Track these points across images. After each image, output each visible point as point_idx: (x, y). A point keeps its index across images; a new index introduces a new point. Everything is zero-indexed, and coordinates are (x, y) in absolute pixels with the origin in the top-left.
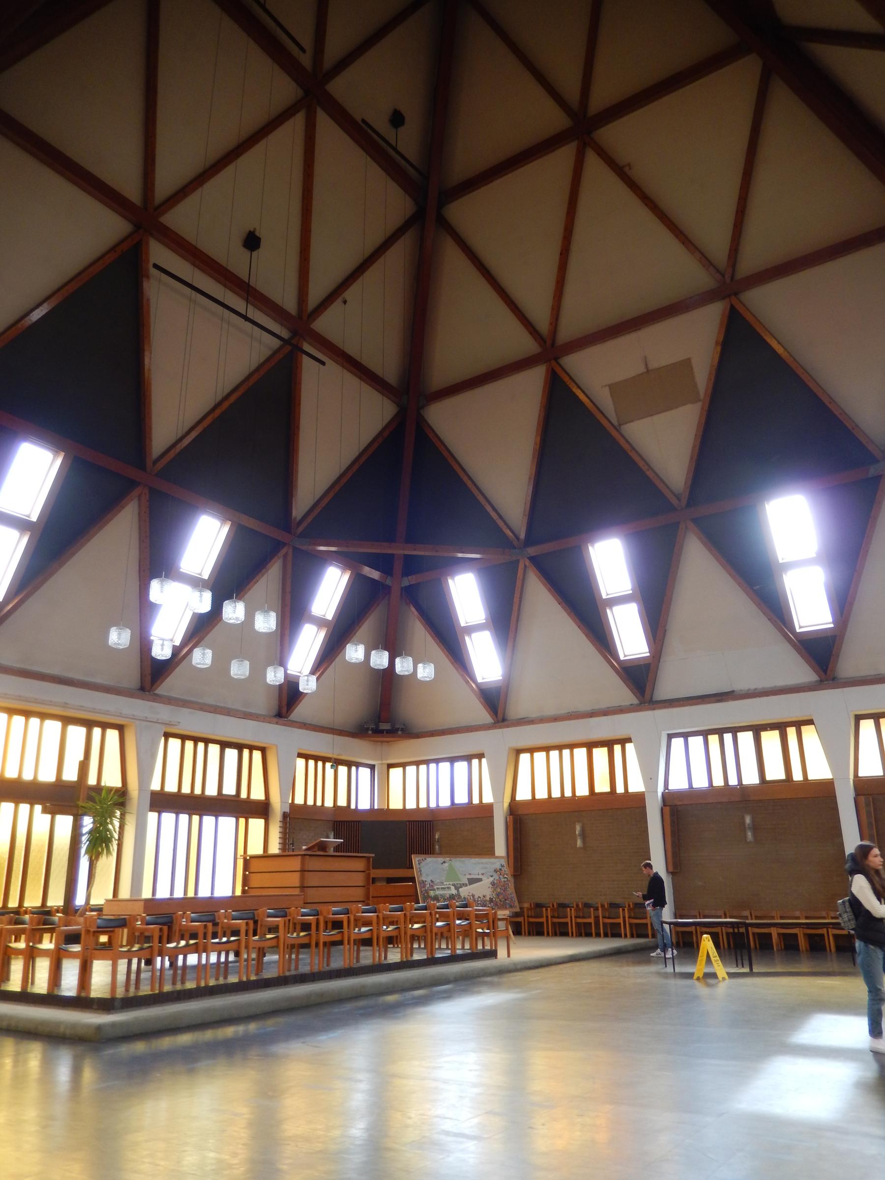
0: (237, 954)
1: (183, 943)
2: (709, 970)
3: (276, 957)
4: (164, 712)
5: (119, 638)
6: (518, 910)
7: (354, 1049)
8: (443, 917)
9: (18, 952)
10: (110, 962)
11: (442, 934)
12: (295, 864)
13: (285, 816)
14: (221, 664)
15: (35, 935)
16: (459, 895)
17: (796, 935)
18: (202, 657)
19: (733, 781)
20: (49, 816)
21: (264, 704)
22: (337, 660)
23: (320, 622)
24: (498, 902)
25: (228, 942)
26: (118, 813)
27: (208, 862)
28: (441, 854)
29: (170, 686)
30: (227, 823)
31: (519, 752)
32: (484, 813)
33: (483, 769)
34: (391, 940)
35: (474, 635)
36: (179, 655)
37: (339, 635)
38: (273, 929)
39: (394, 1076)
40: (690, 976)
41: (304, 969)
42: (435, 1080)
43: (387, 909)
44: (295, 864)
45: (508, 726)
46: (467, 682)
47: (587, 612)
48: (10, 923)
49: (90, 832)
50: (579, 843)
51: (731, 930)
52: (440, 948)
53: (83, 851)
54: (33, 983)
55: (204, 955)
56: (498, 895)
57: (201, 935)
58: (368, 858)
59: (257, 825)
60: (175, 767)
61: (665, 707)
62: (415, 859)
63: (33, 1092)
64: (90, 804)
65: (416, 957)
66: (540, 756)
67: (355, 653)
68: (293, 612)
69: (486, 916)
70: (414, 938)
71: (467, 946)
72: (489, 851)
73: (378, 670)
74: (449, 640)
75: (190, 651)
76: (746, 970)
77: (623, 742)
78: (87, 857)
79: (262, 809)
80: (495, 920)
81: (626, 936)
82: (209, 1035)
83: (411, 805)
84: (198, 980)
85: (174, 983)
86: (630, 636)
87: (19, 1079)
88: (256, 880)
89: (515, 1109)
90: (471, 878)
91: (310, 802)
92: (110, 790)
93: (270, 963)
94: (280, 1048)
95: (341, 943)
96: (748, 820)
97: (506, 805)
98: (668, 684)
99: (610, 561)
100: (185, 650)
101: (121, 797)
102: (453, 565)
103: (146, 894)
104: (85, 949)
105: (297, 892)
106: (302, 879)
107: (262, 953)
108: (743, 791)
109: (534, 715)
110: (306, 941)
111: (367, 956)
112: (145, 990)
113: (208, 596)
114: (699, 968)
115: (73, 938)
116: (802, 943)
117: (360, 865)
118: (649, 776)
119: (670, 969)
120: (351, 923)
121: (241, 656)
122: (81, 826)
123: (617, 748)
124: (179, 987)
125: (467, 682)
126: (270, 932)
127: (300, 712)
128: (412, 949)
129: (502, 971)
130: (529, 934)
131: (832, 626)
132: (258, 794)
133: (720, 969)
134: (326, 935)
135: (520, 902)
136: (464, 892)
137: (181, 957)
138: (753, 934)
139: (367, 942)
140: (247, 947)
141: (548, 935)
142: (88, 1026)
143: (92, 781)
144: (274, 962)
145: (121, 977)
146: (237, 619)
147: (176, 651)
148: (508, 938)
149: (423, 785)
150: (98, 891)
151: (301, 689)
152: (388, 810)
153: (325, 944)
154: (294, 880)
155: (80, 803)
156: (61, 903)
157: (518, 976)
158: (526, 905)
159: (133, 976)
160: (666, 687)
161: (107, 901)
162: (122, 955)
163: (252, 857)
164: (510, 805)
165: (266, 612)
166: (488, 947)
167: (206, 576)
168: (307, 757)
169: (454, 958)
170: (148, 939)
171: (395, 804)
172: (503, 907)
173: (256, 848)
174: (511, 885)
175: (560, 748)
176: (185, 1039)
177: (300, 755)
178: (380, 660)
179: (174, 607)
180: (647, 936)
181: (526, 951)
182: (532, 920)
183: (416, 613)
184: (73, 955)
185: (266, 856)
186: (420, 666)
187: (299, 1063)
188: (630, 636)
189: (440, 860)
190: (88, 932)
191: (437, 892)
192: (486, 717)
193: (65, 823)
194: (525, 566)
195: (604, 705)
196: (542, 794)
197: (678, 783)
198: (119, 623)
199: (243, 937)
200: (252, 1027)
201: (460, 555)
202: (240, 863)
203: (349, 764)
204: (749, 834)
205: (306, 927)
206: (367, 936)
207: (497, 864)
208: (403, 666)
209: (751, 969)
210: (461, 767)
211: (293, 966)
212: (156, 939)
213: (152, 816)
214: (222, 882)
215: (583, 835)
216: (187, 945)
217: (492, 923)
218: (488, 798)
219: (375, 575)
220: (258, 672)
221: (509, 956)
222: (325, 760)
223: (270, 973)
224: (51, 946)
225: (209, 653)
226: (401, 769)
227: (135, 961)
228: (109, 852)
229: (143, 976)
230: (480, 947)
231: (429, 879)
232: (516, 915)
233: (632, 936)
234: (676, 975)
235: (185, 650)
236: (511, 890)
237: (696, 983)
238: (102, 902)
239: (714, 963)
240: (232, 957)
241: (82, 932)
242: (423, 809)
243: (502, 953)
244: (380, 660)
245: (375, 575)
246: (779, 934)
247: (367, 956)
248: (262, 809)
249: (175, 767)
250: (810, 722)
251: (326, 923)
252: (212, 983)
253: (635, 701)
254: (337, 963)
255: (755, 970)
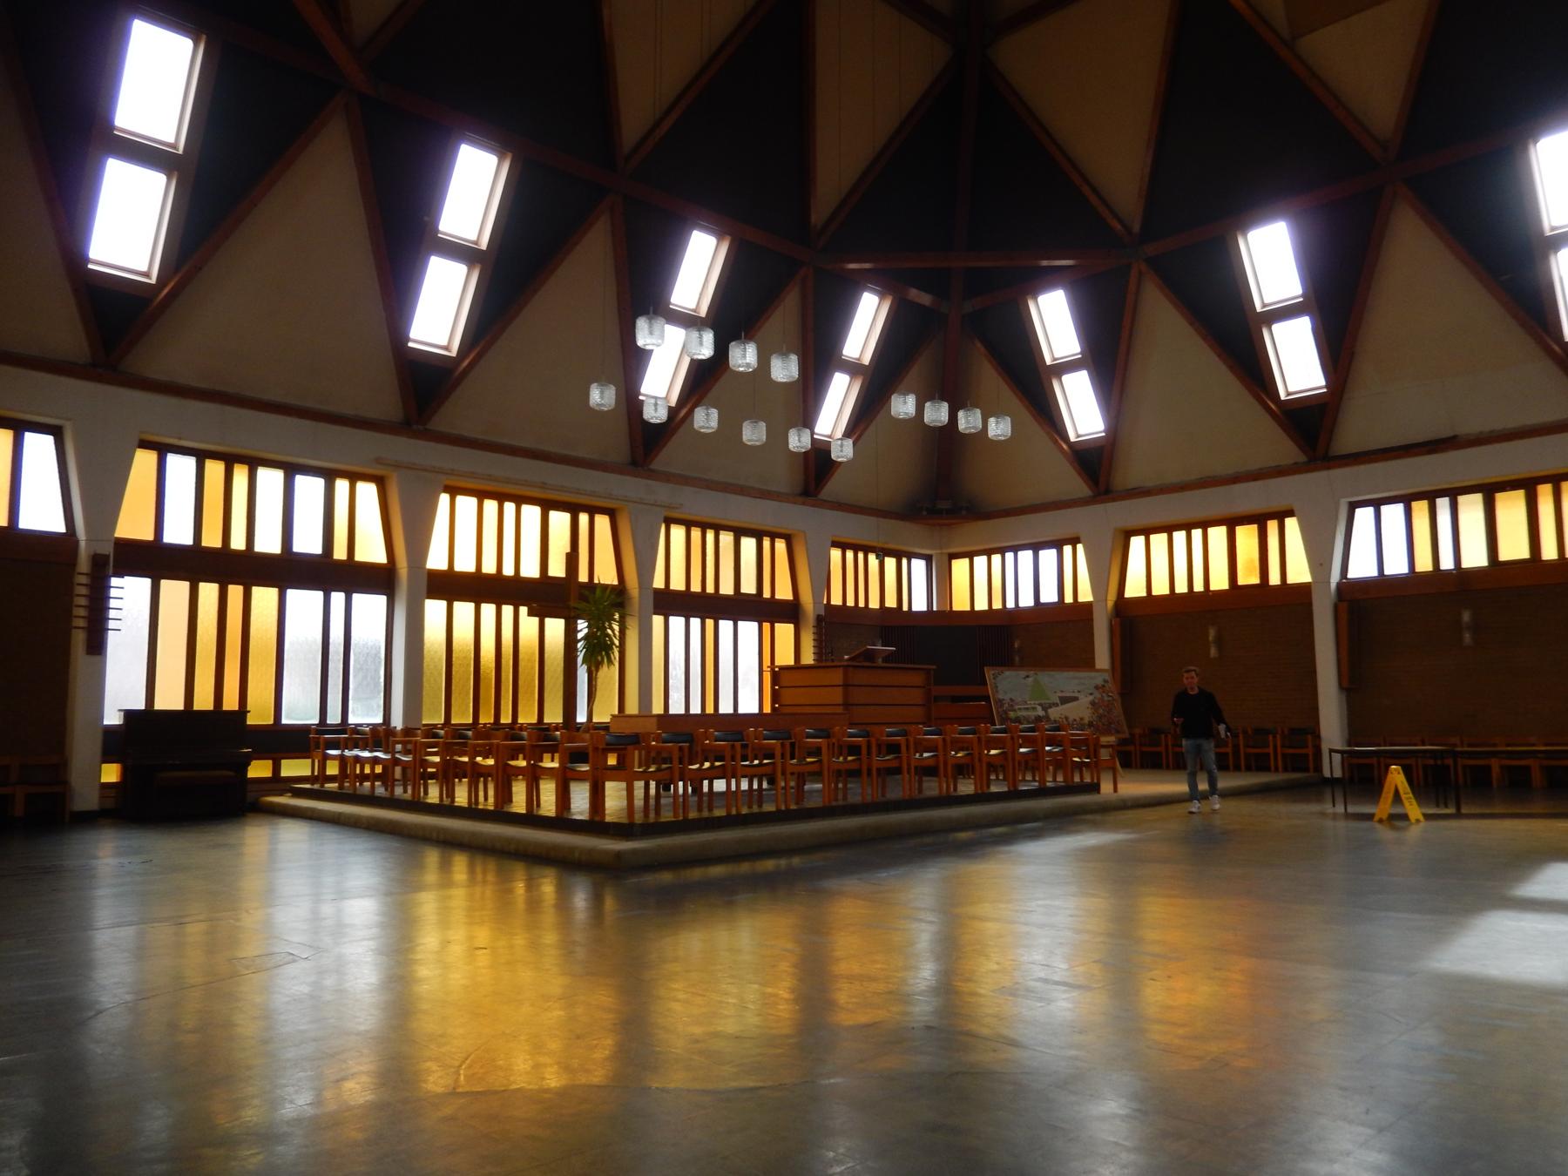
0: (772, 782)
1: (707, 765)
2: (1398, 810)
3: (819, 786)
4: (663, 492)
5: (601, 397)
6: (1127, 735)
7: (919, 893)
8: (1027, 742)
9: (520, 770)
10: (624, 785)
11: (1026, 763)
12: (837, 677)
13: (819, 619)
14: (730, 427)
15: (535, 754)
16: (1047, 718)
17: (1527, 768)
18: (706, 419)
19: (1447, 563)
20: (536, 620)
21: (784, 478)
22: (879, 418)
23: (853, 368)
24: (1102, 724)
25: (761, 764)
26: (617, 616)
27: (737, 671)
28: (1022, 666)
29: (670, 457)
30: (749, 629)
31: (1128, 534)
32: (1082, 612)
33: (1078, 559)
34: (962, 770)
35: (1067, 379)
36: (680, 414)
37: (878, 383)
38: (817, 752)
39: (974, 918)
40: (1370, 817)
41: (855, 798)
42: (1026, 924)
43: (957, 731)
44: (837, 677)
45: (1114, 500)
46: (1056, 442)
47: (1238, 337)
48: (506, 739)
49: (586, 638)
50: (1213, 652)
51: (1431, 762)
52: (1024, 780)
53: (580, 659)
54: (538, 805)
55: (733, 782)
56: (1100, 717)
57: (728, 757)
58: (928, 671)
59: (785, 631)
60: (678, 558)
61: (1347, 465)
62: (989, 673)
63: (549, 916)
64: (583, 605)
65: (994, 789)
66: (1159, 540)
67: (903, 406)
68: (820, 357)
69: (1085, 742)
70: (992, 766)
71: (1060, 778)
72: (1088, 663)
73: (934, 428)
74: (1032, 384)
75: (691, 412)
76: (1451, 810)
77: (1281, 516)
78: (585, 667)
79: (789, 612)
80: (1098, 746)
81: (1276, 770)
82: (745, 867)
83: (981, 605)
84: (728, 809)
85: (700, 809)
86: (1297, 360)
87: (534, 905)
88: (788, 697)
89: (1121, 965)
90: (1072, 696)
91: (696, 587)
92: (605, 587)
93: (811, 792)
94: (832, 884)
95: (898, 771)
96: (1466, 617)
97: (1110, 604)
98: (1352, 433)
99: (1271, 258)
100: (683, 412)
101: (617, 597)
102: (1038, 281)
103: (658, 709)
104: (594, 768)
105: (840, 710)
106: (846, 695)
107: (802, 779)
108: (1461, 575)
109: (1149, 484)
110: (854, 766)
111: (932, 787)
112: (667, 816)
113: (709, 337)
114: (1384, 808)
115: (581, 756)
116: (1537, 777)
117: (918, 679)
118: (1318, 556)
119: (1340, 809)
120: (904, 749)
121: (755, 417)
122: (576, 631)
123: (1272, 526)
124: (706, 814)
125: (1056, 442)
126: (810, 755)
127: (834, 487)
128: (989, 780)
129: (1107, 809)
130: (1142, 767)
131: (1048, 361)
132: (784, 593)
133: (1413, 810)
134: (880, 760)
135: (1130, 727)
136: (1054, 713)
137: (706, 783)
138: (1464, 767)
139: (930, 771)
140: (784, 773)
141: (1168, 768)
142: (606, 852)
143: (583, 577)
144: (817, 791)
145: (639, 801)
146: (748, 365)
147: (672, 412)
148: (1114, 770)
149: (1024, 577)
150: (600, 706)
151: (833, 456)
152: (952, 612)
153: (878, 770)
154: (837, 696)
155: (572, 604)
156: (560, 720)
157: (1130, 814)
158: (1137, 731)
159: (652, 802)
160: (1350, 437)
161: (614, 716)
162: (638, 776)
163: (782, 668)
164: (1339, 585)
165: (784, 354)
166: (1088, 779)
167: (703, 312)
168: (844, 547)
169: (1042, 792)
170: (668, 760)
171: (960, 603)
172: (1108, 732)
173: (785, 657)
174: (1118, 705)
175: (1188, 527)
176: (717, 871)
177: (835, 544)
178: (937, 414)
179: (666, 358)
180: (1307, 770)
181: (1135, 786)
182: (1145, 749)
183: (983, 349)
184: (580, 778)
185: (798, 667)
186: (992, 421)
187: (849, 907)
188: (1297, 360)
189: (1023, 673)
190: (596, 749)
191: (1020, 714)
192: (1080, 488)
193: (555, 628)
194: (1140, 273)
195: (1254, 465)
196: (1161, 588)
197: (1362, 566)
198: (603, 380)
199: (779, 760)
200: (796, 861)
201: (1045, 263)
202: (767, 677)
203: (898, 555)
204: (1467, 637)
205: (854, 749)
206: (932, 762)
207: (1099, 679)
208: (968, 421)
209: (1458, 809)
210: (1048, 556)
211: (840, 796)
212: (676, 760)
213: (658, 621)
214: (747, 697)
215: (1219, 640)
216: (712, 767)
217: (1090, 747)
218: (1086, 595)
219: (925, 299)
220: (777, 437)
221: (1115, 790)
222: (867, 550)
223: (813, 803)
224: (555, 765)
225: (714, 413)
226: (966, 561)
227: (653, 784)
228: (610, 662)
229: (663, 801)
230: (1077, 779)
231: (1007, 697)
232: (1123, 742)
233: (1286, 770)
234: (1347, 816)
235: (683, 412)
236: (1118, 711)
237: (1378, 826)
238: (607, 720)
239: (1406, 803)
240: (765, 785)
241: (585, 750)
242: (1396, 580)
243: (1106, 787)
244: (937, 414)
245: (925, 299)
246: (1502, 767)
247: (932, 787)
248: (789, 612)
249: (678, 558)
250: (1291, 513)
251: (879, 746)
252: (745, 811)
253: (1302, 458)
254: (895, 793)
255: (1464, 811)
